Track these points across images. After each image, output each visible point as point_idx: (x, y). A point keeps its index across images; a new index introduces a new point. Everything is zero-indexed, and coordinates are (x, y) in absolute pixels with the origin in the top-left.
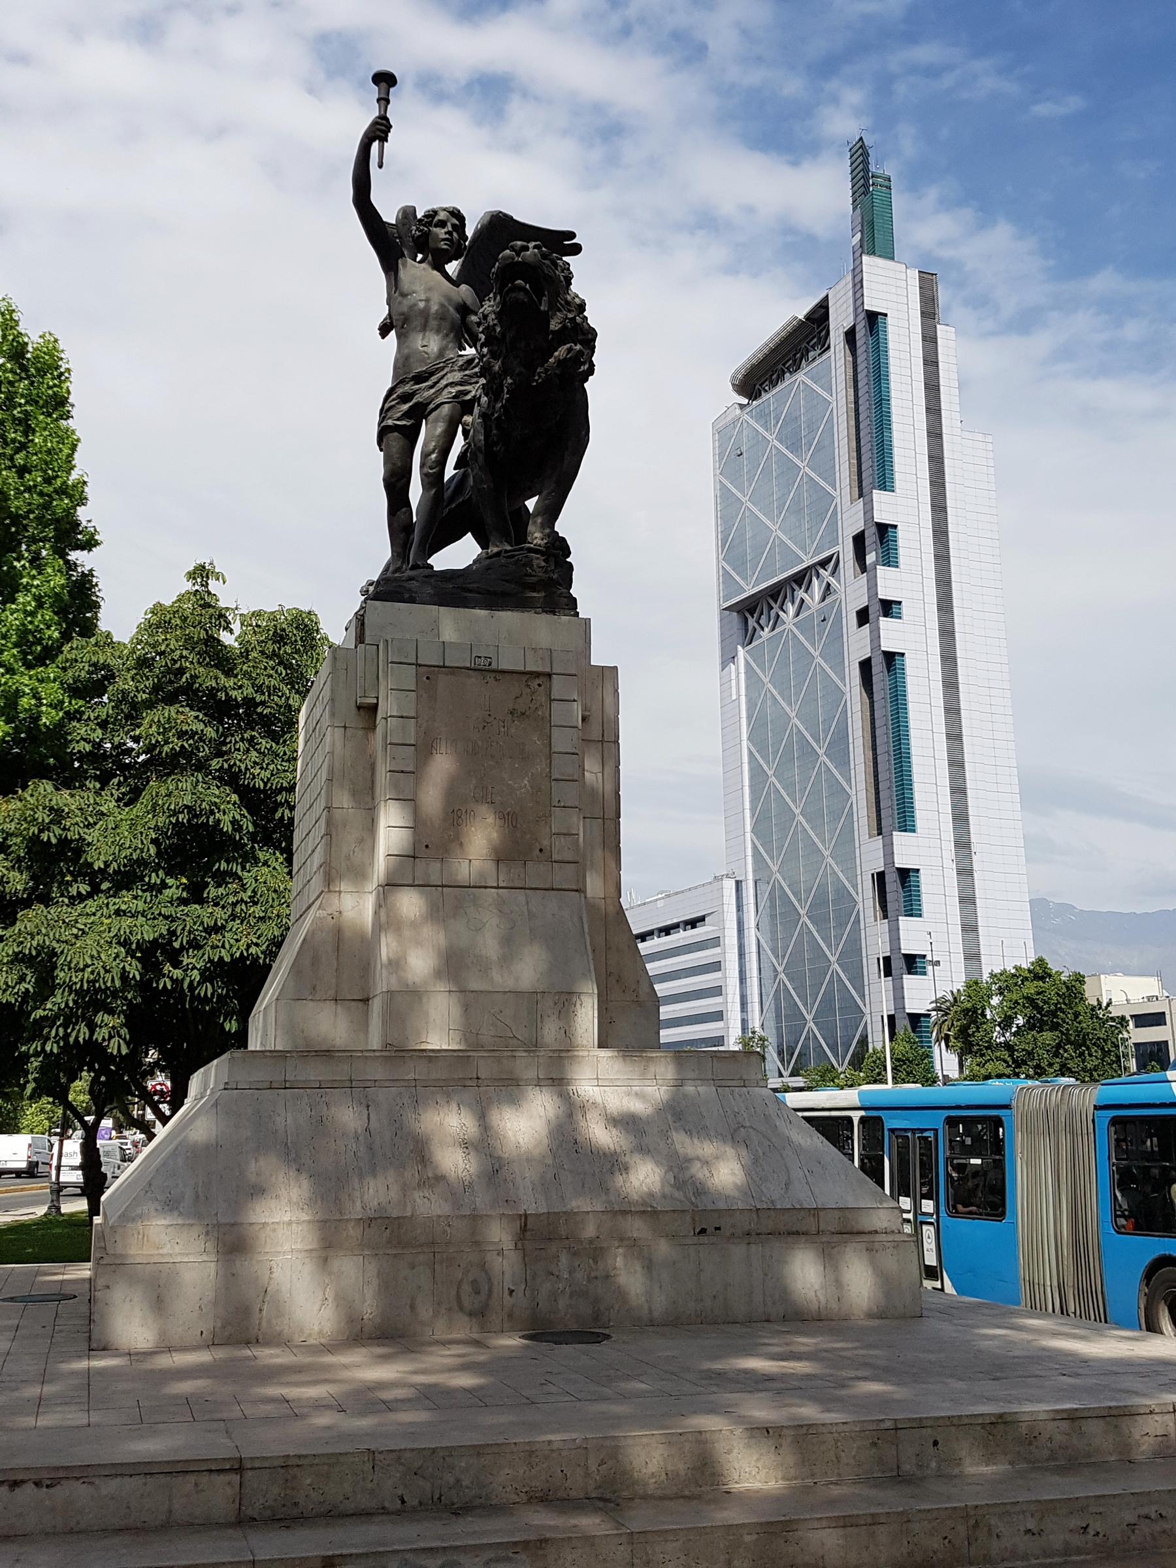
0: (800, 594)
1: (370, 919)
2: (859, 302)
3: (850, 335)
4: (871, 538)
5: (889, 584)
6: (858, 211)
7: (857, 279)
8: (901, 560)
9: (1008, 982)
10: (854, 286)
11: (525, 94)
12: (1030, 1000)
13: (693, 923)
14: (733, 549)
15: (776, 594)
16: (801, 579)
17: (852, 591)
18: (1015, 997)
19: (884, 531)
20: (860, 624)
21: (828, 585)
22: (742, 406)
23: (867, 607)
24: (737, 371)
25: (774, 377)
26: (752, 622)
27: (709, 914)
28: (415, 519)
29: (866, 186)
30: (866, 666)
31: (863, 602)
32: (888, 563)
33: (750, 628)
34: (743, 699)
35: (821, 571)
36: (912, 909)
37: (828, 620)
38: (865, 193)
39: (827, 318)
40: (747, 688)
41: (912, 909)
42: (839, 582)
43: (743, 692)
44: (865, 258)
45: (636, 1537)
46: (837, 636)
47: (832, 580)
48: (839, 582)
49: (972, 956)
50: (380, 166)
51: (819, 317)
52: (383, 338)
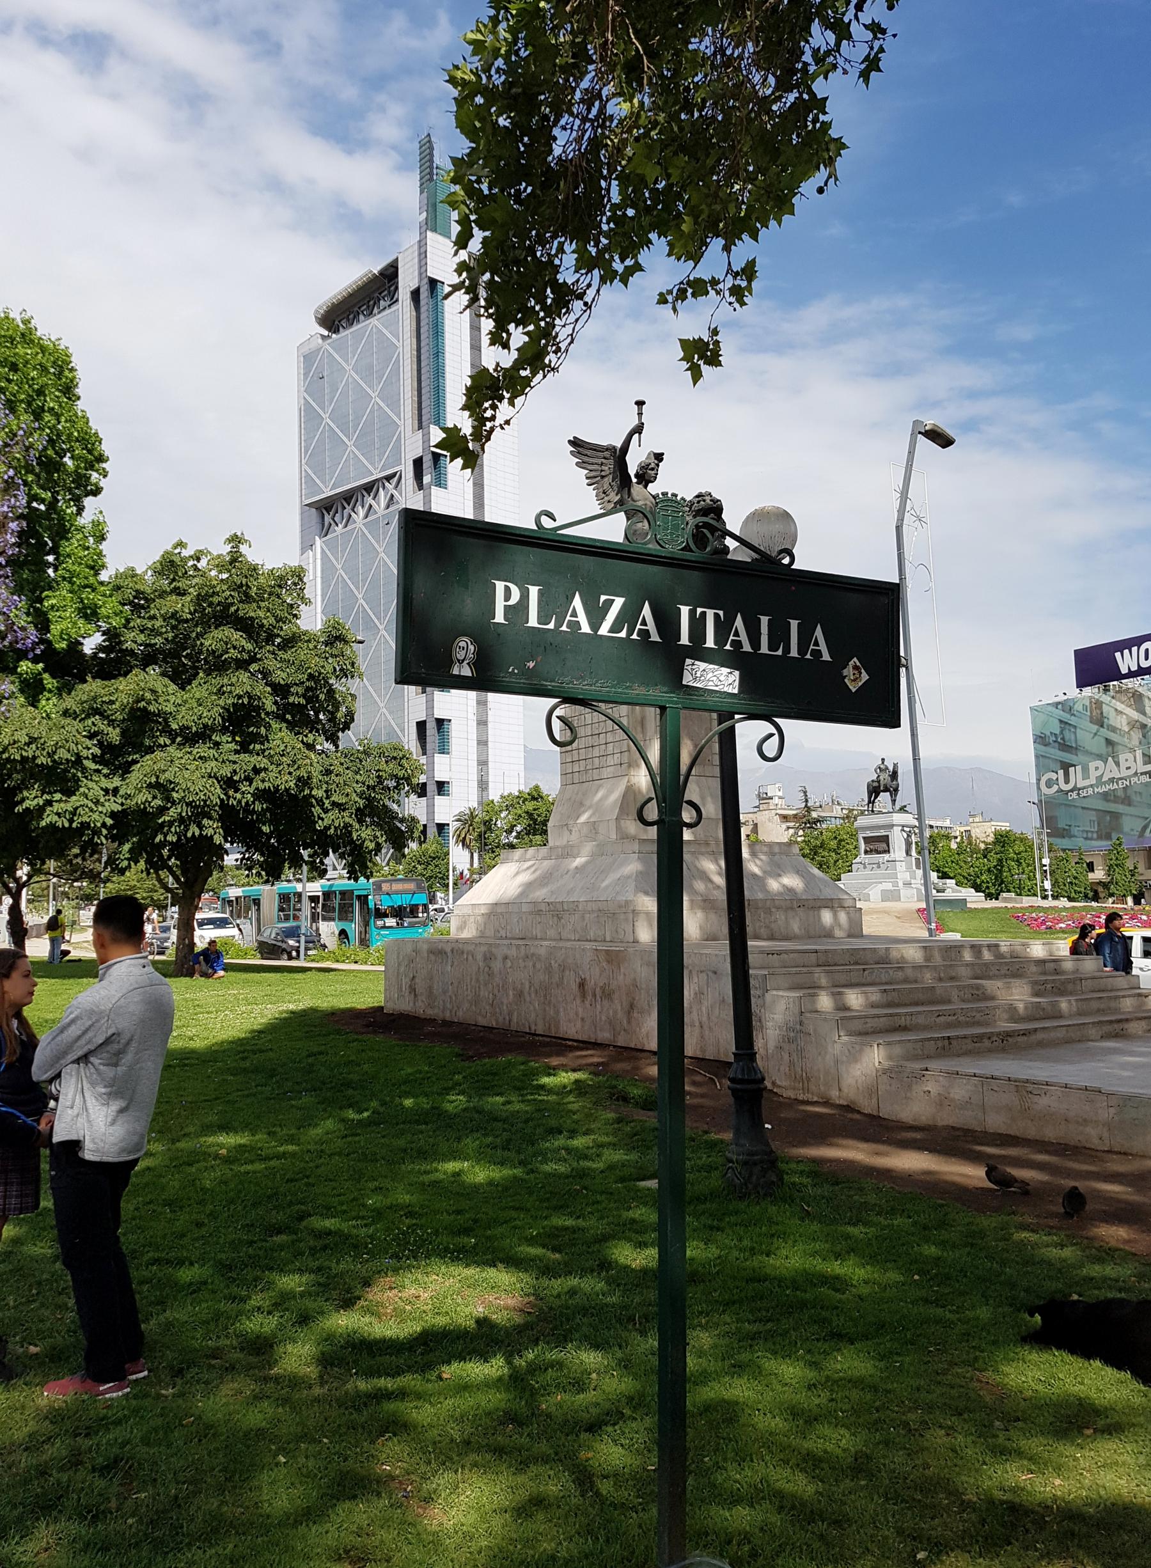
0: (369, 500)
2: (423, 269)
3: (415, 294)
4: (427, 463)
6: (425, 194)
7: (423, 250)
8: (449, 483)
9: (511, 802)
10: (420, 254)
11: (123, 54)
12: (530, 815)
14: (314, 454)
15: (349, 497)
16: (369, 488)
18: (519, 812)
21: (392, 496)
22: (323, 337)
24: (320, 307)
25: (351, 316)
26: (328, 518)
29: (431, 174)
32: (439, 485)
33: (326, 524)
34: (319, 580)
35: (387, 484)
36: (444, 749)
38: (431, 180)
39: (397, 276)
40: (322, 571)
41: (444, 749)
42: (401, 494)
43: (319, 574)
44: (429, 233)
45: (954, 1042)
47: (395, 493)
48: (401, 494)
49: (483, 785)
51: (389, 276)
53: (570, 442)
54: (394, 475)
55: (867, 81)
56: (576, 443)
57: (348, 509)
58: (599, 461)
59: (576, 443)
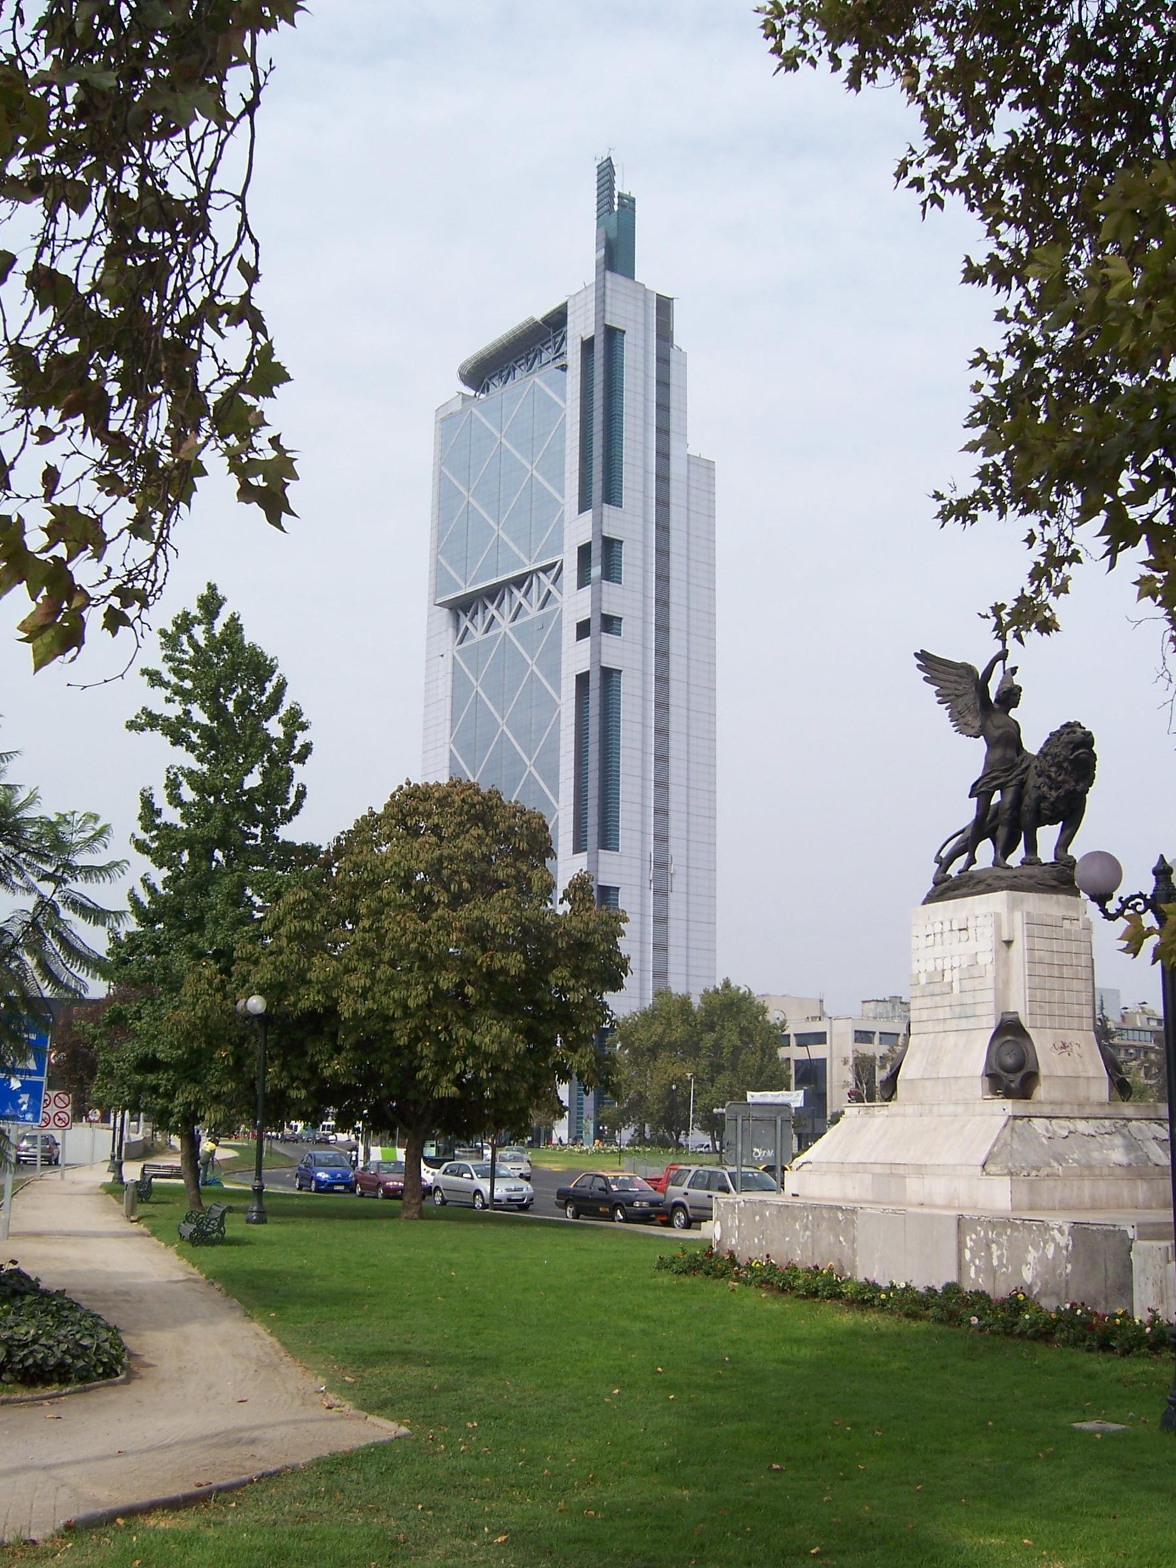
0: (518, 594)
3: (587, 346)
4: (596, 552)
5: (615, 600)
14: (453, 533)
15: (493, 594)
17: (576, 603)
19: (610, 546)
20: (582, 509)
22: (465, 398)
24: (469, 361)
28: (753, 1097)
30: (582, 680)
31: (585, 614)
35: (515, 591)
37: (549, 625)
46: (555, 645)
51: (557, 321)
52: (206, 474)
53: (916, 654)
54: (553, 565)
55: (1008, 133)
56: (923, 656)
57: (492, 608)
58: (953, 678)
59: (923, 656)
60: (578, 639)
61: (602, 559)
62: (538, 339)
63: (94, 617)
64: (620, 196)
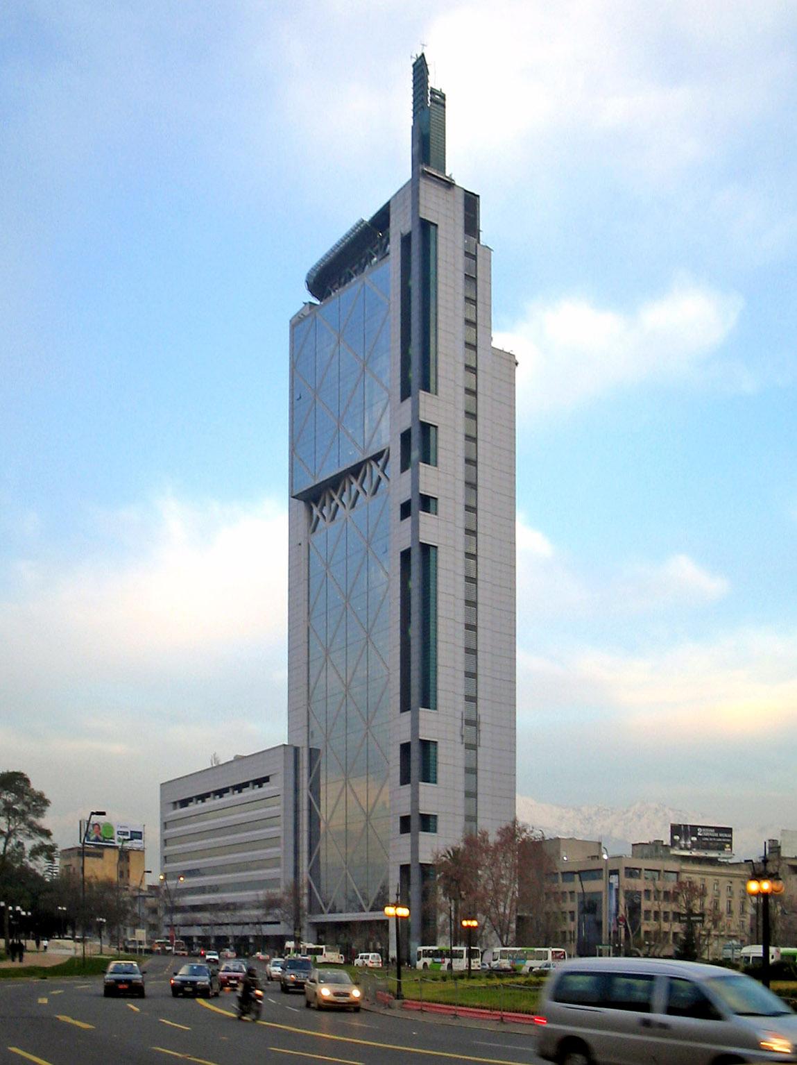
1: (647, 981)
3: (406, 240)
4: (415, 875)
5: (430, 480)
11: (101, 996)
13: (260, 782)
17: (399, 487)
20: (403, 398)
23: (410, 500)
26: (316, 511)
27: (271, 775)
30: (406, 556)
33: (315, 518)
35: (353, 480)
50: (103, 814)
60: (402, 519)
61: (419, 443)
62: (366, 241)
63: (47, 842)
64: (433, 92)
